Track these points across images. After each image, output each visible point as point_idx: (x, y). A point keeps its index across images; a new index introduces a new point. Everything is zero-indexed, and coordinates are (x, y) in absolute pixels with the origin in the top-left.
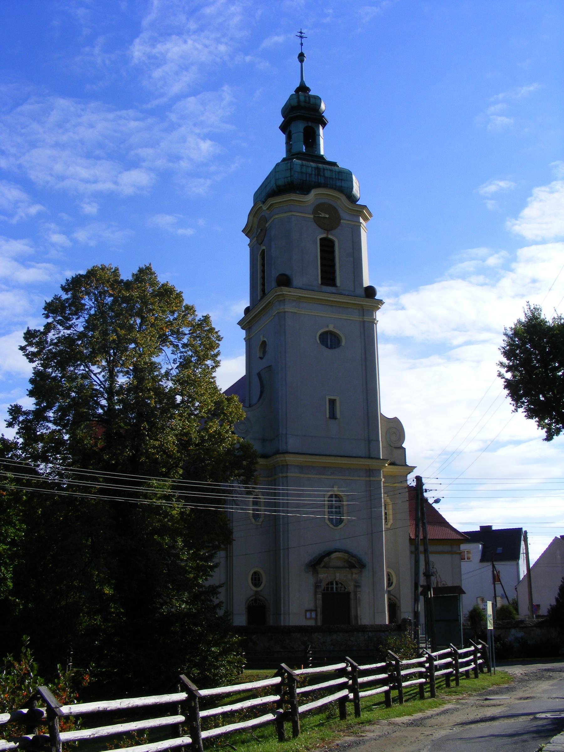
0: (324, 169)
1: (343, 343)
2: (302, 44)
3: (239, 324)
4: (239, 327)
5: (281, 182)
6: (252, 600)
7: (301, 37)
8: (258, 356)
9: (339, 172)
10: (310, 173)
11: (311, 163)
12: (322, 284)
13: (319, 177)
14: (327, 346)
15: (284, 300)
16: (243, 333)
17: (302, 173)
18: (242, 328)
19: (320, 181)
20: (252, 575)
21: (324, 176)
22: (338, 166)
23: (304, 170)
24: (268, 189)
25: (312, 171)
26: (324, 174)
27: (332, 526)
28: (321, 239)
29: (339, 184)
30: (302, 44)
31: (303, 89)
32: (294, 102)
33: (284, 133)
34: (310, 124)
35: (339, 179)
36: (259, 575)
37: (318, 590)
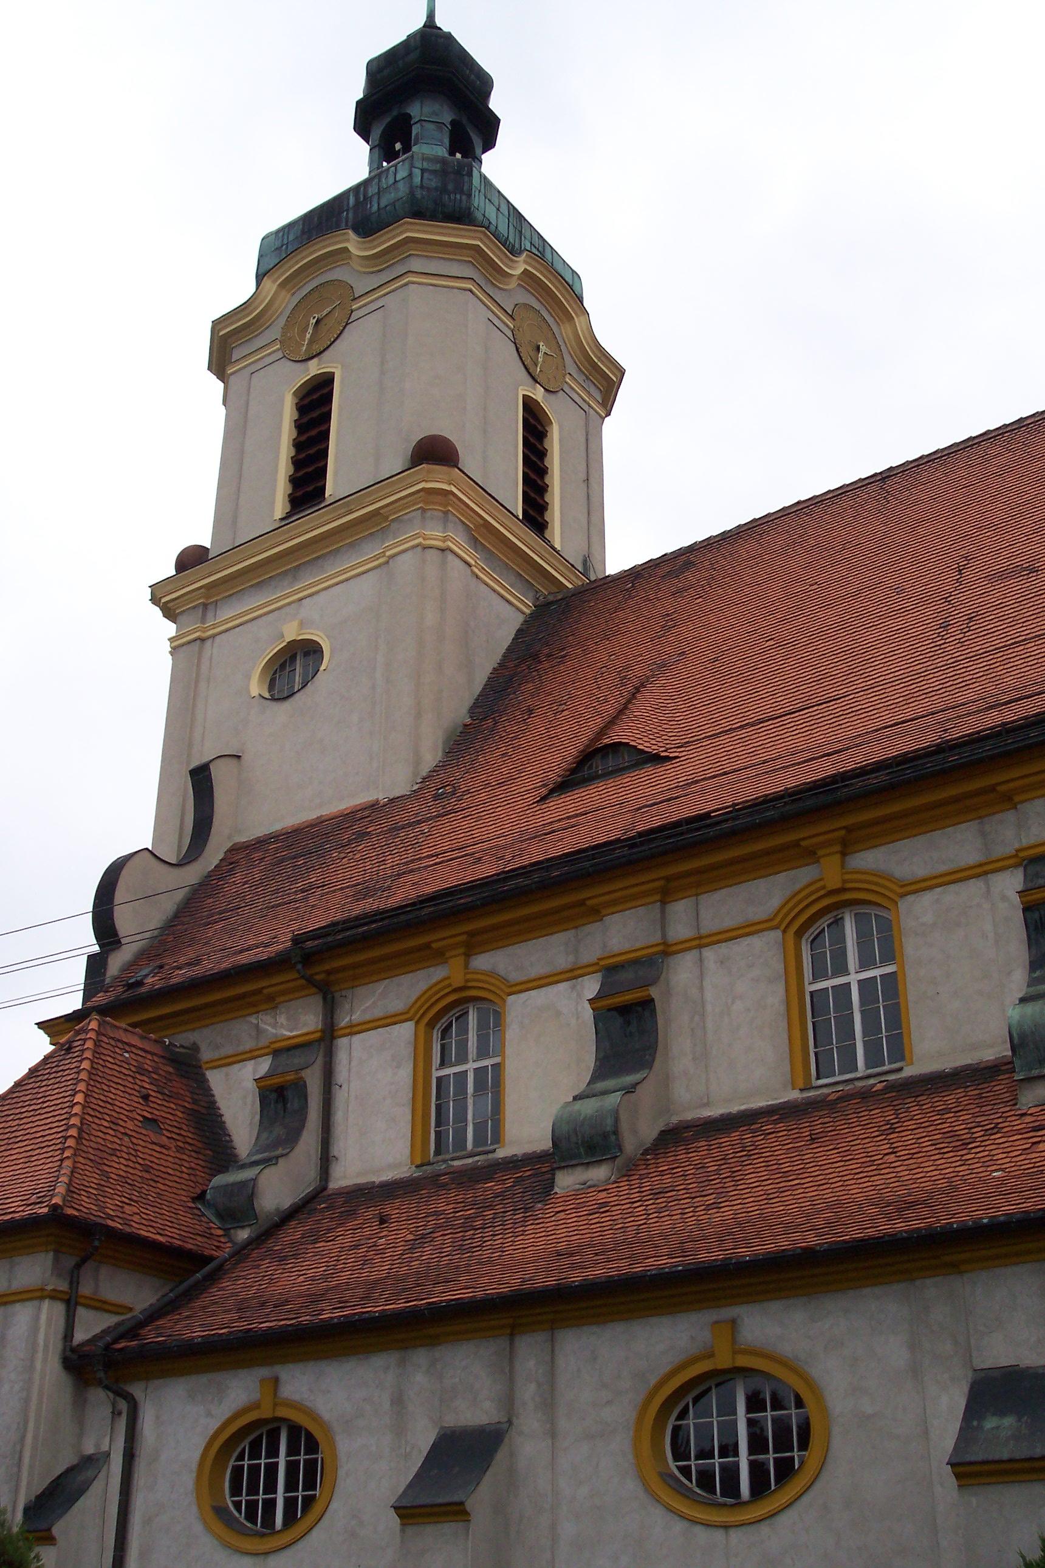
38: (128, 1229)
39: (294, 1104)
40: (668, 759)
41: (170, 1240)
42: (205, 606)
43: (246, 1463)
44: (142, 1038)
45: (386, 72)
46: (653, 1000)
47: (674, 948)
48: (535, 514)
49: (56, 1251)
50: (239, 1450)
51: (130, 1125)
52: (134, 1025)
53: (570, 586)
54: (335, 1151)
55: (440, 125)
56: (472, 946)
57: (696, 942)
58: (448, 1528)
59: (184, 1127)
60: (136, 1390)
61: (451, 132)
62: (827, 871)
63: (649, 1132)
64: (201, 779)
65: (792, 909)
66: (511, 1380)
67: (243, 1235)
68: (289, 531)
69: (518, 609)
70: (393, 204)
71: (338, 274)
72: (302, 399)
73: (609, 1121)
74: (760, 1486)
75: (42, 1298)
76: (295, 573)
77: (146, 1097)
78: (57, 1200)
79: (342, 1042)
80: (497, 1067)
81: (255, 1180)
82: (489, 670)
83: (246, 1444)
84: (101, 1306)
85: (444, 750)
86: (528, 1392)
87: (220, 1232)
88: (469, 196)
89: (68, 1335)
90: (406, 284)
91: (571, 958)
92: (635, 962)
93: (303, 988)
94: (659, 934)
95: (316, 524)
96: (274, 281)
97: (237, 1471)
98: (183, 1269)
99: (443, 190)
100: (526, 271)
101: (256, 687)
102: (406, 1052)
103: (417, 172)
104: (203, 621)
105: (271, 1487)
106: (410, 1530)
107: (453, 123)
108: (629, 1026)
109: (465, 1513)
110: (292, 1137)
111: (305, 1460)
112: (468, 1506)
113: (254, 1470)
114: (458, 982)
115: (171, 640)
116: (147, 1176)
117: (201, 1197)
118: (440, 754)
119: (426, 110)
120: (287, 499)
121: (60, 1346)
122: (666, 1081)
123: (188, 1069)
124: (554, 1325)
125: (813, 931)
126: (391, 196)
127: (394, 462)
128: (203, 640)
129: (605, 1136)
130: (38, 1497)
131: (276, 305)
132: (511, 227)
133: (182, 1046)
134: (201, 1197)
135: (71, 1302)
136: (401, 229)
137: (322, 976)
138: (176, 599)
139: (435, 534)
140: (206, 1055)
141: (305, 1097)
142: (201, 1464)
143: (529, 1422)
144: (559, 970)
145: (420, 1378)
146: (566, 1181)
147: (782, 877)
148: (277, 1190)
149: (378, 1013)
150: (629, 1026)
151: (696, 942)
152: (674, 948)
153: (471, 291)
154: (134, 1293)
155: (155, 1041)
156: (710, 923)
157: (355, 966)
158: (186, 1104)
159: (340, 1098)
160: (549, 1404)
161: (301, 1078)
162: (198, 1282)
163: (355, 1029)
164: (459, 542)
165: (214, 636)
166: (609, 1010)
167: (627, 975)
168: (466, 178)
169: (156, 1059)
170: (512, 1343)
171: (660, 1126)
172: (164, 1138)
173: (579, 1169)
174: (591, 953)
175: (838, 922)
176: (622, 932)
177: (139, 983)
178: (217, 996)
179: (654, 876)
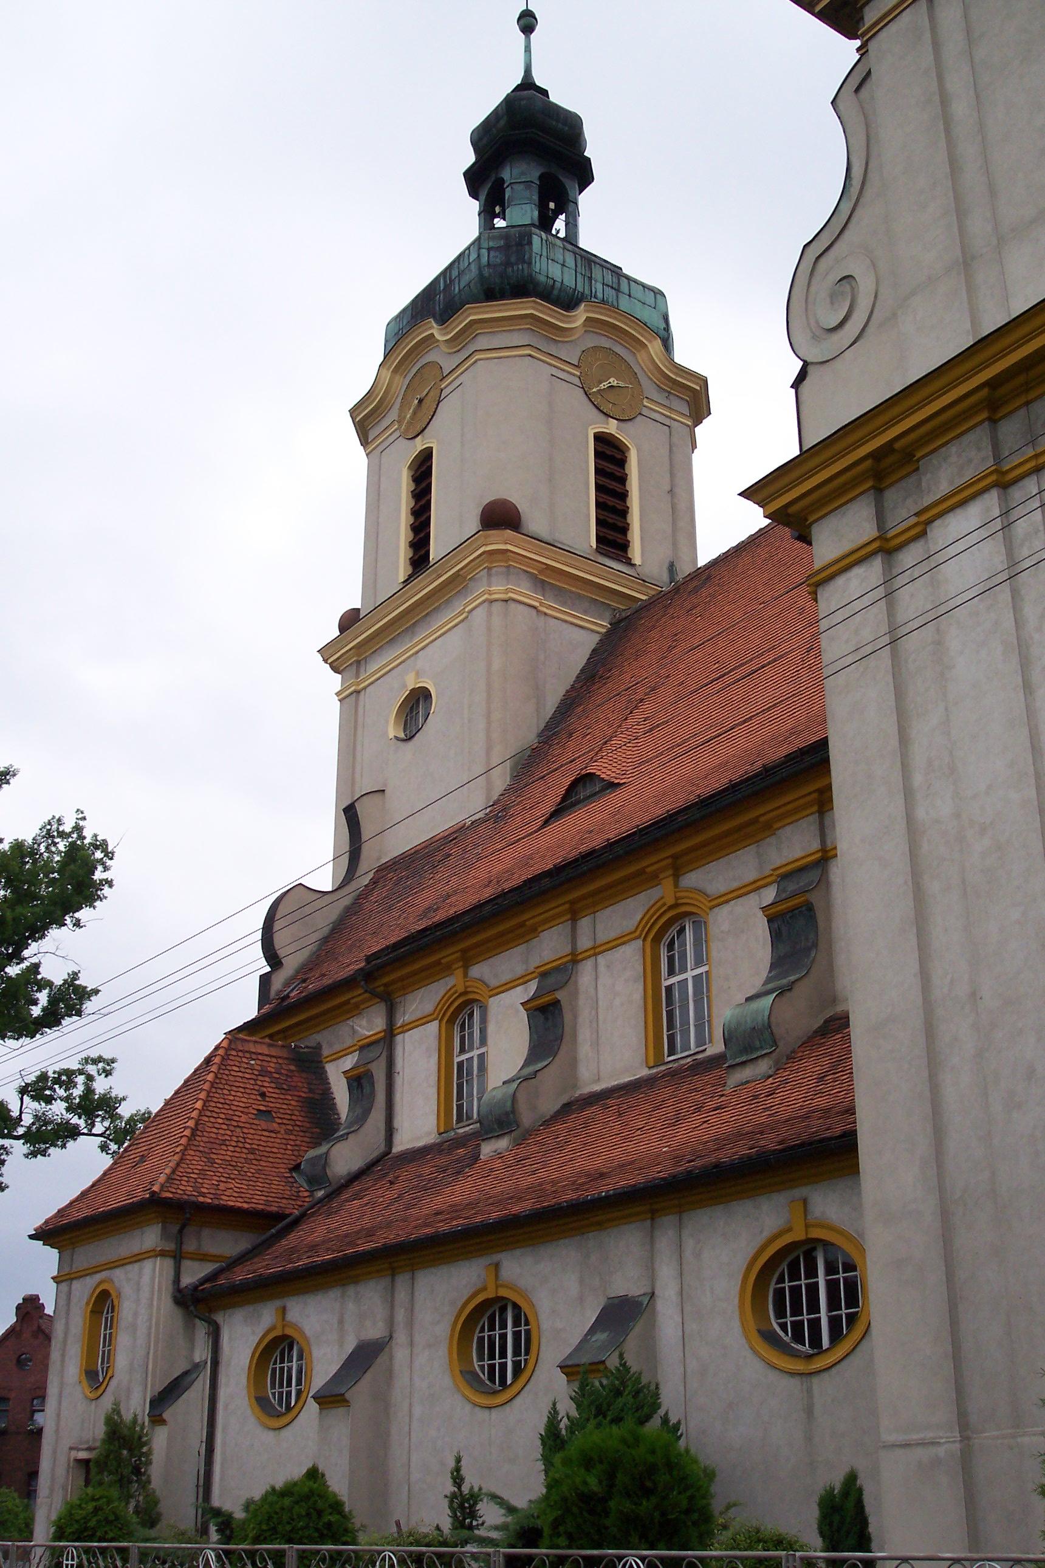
8: (391, 736)
31: (527, 84)
38: (216, 1202)
39: (367, 1090)
40: (619, 784)
41: (254, 1206)
42: (358, 662)
43: (787, 1285)
44: (270, 1045)
45: (485, 141)
46: (559, 1001)
47: (580, 957)
48: (613, 535)
49: (163, 1223)
50: (780, 1270)
51: (244, 1118)
52: (271, 1036)
53: (644, 598)
54: (397, 1123)
55: (528, 184)
56: (467, 960)
57: (592, 952)
58: (341, 1410)
59: (297, 1113)
60: (219, 1318)
61: (540, 187)
62: (663, 892)
63: (549, 1105)
64: (350, 815)
65: (647, 923)
66: (392, 1307)
67: (320, 1194)
68: (401, 596)
69: (592, 631)
70: (468, 285)
71: (432, 356)
72: (416, 471)
73: (509, 1104)
74: (836, 1335)
75: (156, 1256)
76: (411, 629)
77: (263, 1095)
78: (156, 1188)
79: (399, 1038)
80: (481, 1057)
81: (327, 1153)
82: (561, 691)
83: (784, 1266)
84: (203, 1258)
85: (511, 775)
86: (400, 1316)
87: (306, 1194)
88: (530, 263)
89: (177, 1280)
90: (475, 362)
91: (524, 967)
92: (557, 969)
93: (370, 1000)
94: (570, 947)
95: (427, 584)
96: (388, 369)
97: (779, 1294)
98: (268, 1224)
99: (507, 264)
100: (588, 319)
101: (393, 730)
102: (434, 1044)
103: (484, 252)
104: (357, 676)
105: (814, 1307)
106: (325, 1412)
107: (541, 178)
108: (548, 1018)
109: (348, 1401)
110: (367, 1112)
111: (806, 1285)
112: (347, 1396)
113: (796, 1291)
114: (460, 989)
115: (338, 694)
116: (252, 1157)
117: (297, 1168)
118: (508, 779)
119: (516, 171)
120: (408, 562)
121: (171, 1287)
122: (574, 1063)
123: (311, 1065)
124: (413, 1268)
125: (666, 939)
126: (465, 279)
127: (473, 524)
128: (358, 692)
129: (507, 1114)
130: (160, 1393)
131: (393, 390)
132: (579, 276)
133: (307, 1047)
134: (297, 1168)
135: (178, 1257)
136: (465, 314)
137: (382, 988)
138: (338, 659)
139: (499, 588)
140: (326, 1052)
141: (373, 1084)
142: (249, 1368)
143: (401, 1337)
144: (518, 976)
145: (351, 1306)
146: (487, 1149)
147: (642, 896)
148: (345, 1157)
149: (419, 1015)
150: (548, 1018)
151: (592, 952)
152: (580, 957)
153: (530, 355)
154: (227, 1244)
155: (283, 1046)
156: (603, 937)
157: (402, 979)
158: (303, 1095)
159: (398, 1081)
160: (410, 1324)
161: (369, 1070)
162: (273, 1236)
163: (408, 1027)
164: (524, 591)
165: (365, 688)
166: (536, 1010)
167: (551, 980)
168: (527, 247)
169: (280, 1061)
170: (393, 1281)
171: (565, 1099)
172: (275, 1125)
173: (493, 1140)
174: (535, 962)
175: (682, 930)
176: (549, 946)
177: (287, 996)
178: (302, 1017)
179: (561, 901)
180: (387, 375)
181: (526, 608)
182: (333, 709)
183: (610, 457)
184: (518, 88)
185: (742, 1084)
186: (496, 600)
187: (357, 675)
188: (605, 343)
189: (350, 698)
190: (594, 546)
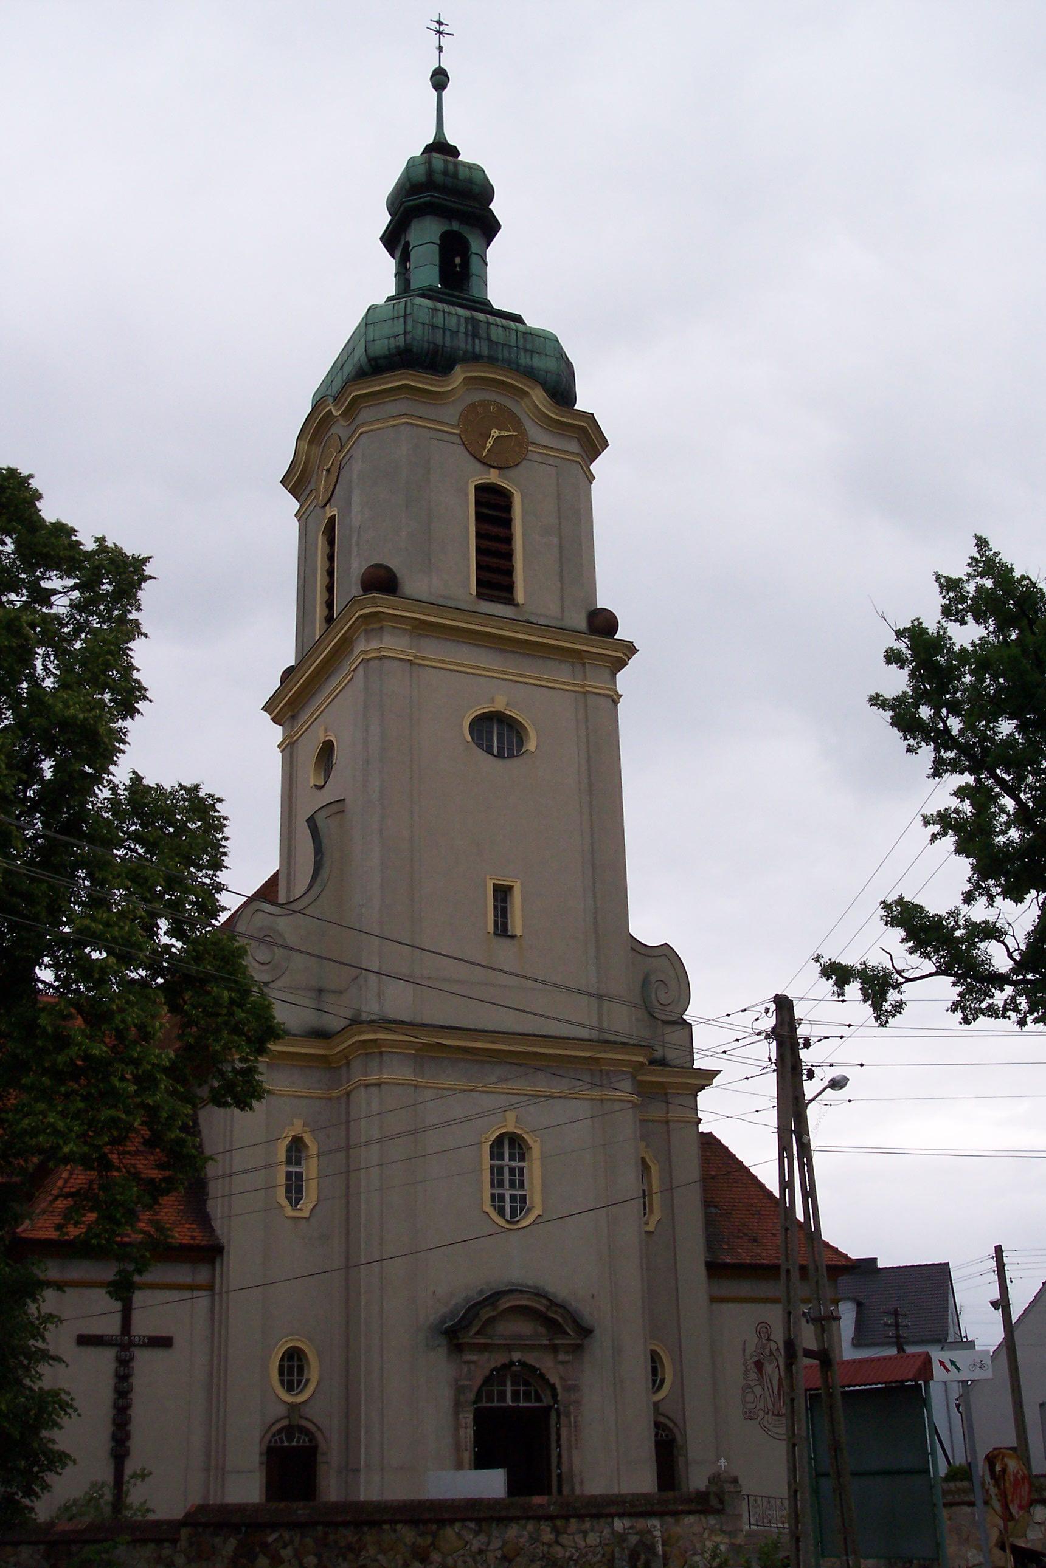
0: (488, 323)
1: (531, 745)
2: (440, 49)
3: (265, 709)
4: (267, 716)
5: (380, 348)
6: (280, 1431)
7: (439, 32)
8: (312, 784)
9: (525, 333)
10: (455, 329)
11: (458, 309)
12: (480, 595)
13: (477, 341)
14: (490, 751)
15: (381, 628)
16: (277, 733)
17: (433, 326)
18: (274, 720)
19: (477, 349)
20: (282, 1359)
21: (489, 339)
22: (523, 323)
23: (439, 320)
24: (348, 369)
25: (458, 325)
26: (488, 334)
27: (502, 1222)
28: (480, 489)
29: (524, 360)
30: (440, 49)
31: (441, 147)
32: (420, 174)
33: (393, 257)
34: (455, 226)
35: (526, 351)
36: (300, 1359)
37: (462, 1399)
107: (442, 237)
115: (279, 746)
180: (305, 444)
181: (397, 663)
182: (275, 760)
183: (493, 508)
184: (429, 149)
185: (212, 1319)
186: (371, 659)
187: (292, 728)
188: (494, 397)
189: (288, 747)
190: (474, 593)
